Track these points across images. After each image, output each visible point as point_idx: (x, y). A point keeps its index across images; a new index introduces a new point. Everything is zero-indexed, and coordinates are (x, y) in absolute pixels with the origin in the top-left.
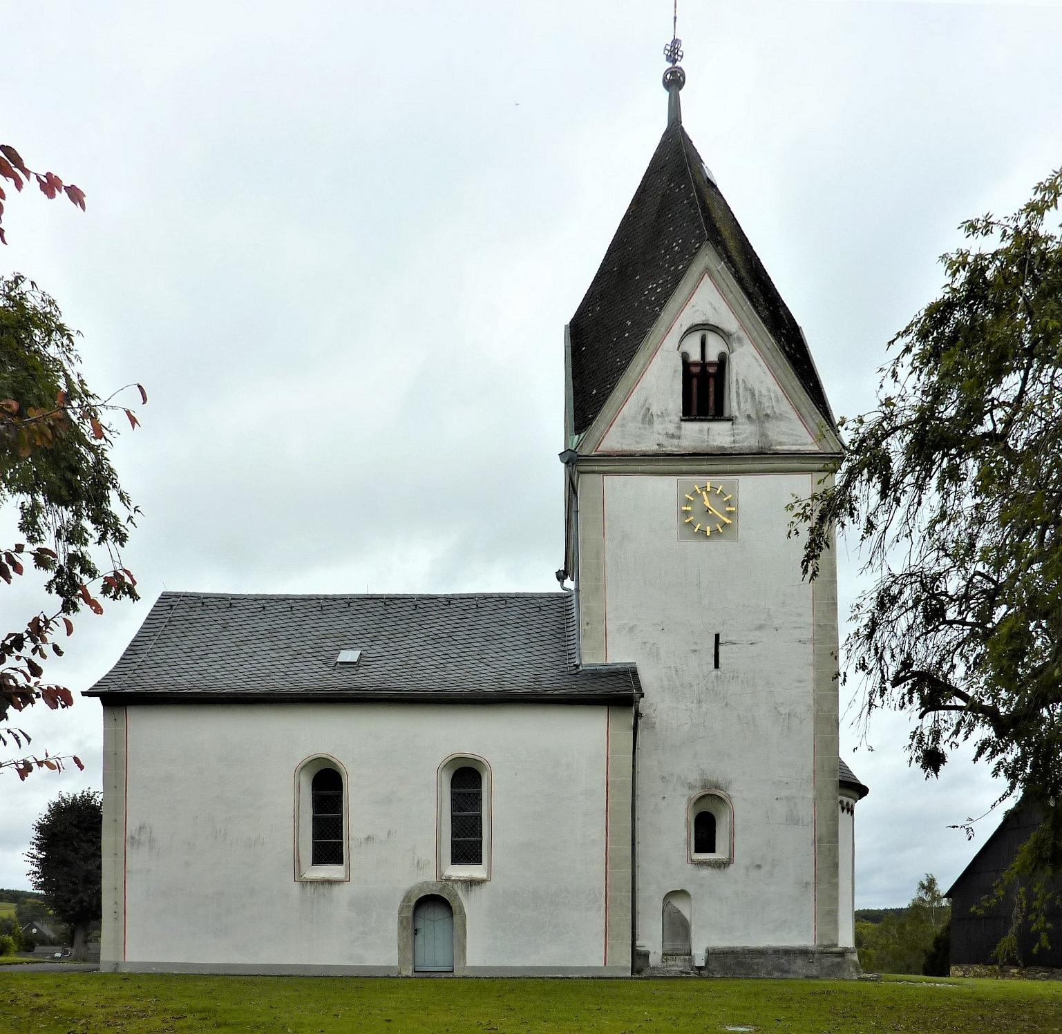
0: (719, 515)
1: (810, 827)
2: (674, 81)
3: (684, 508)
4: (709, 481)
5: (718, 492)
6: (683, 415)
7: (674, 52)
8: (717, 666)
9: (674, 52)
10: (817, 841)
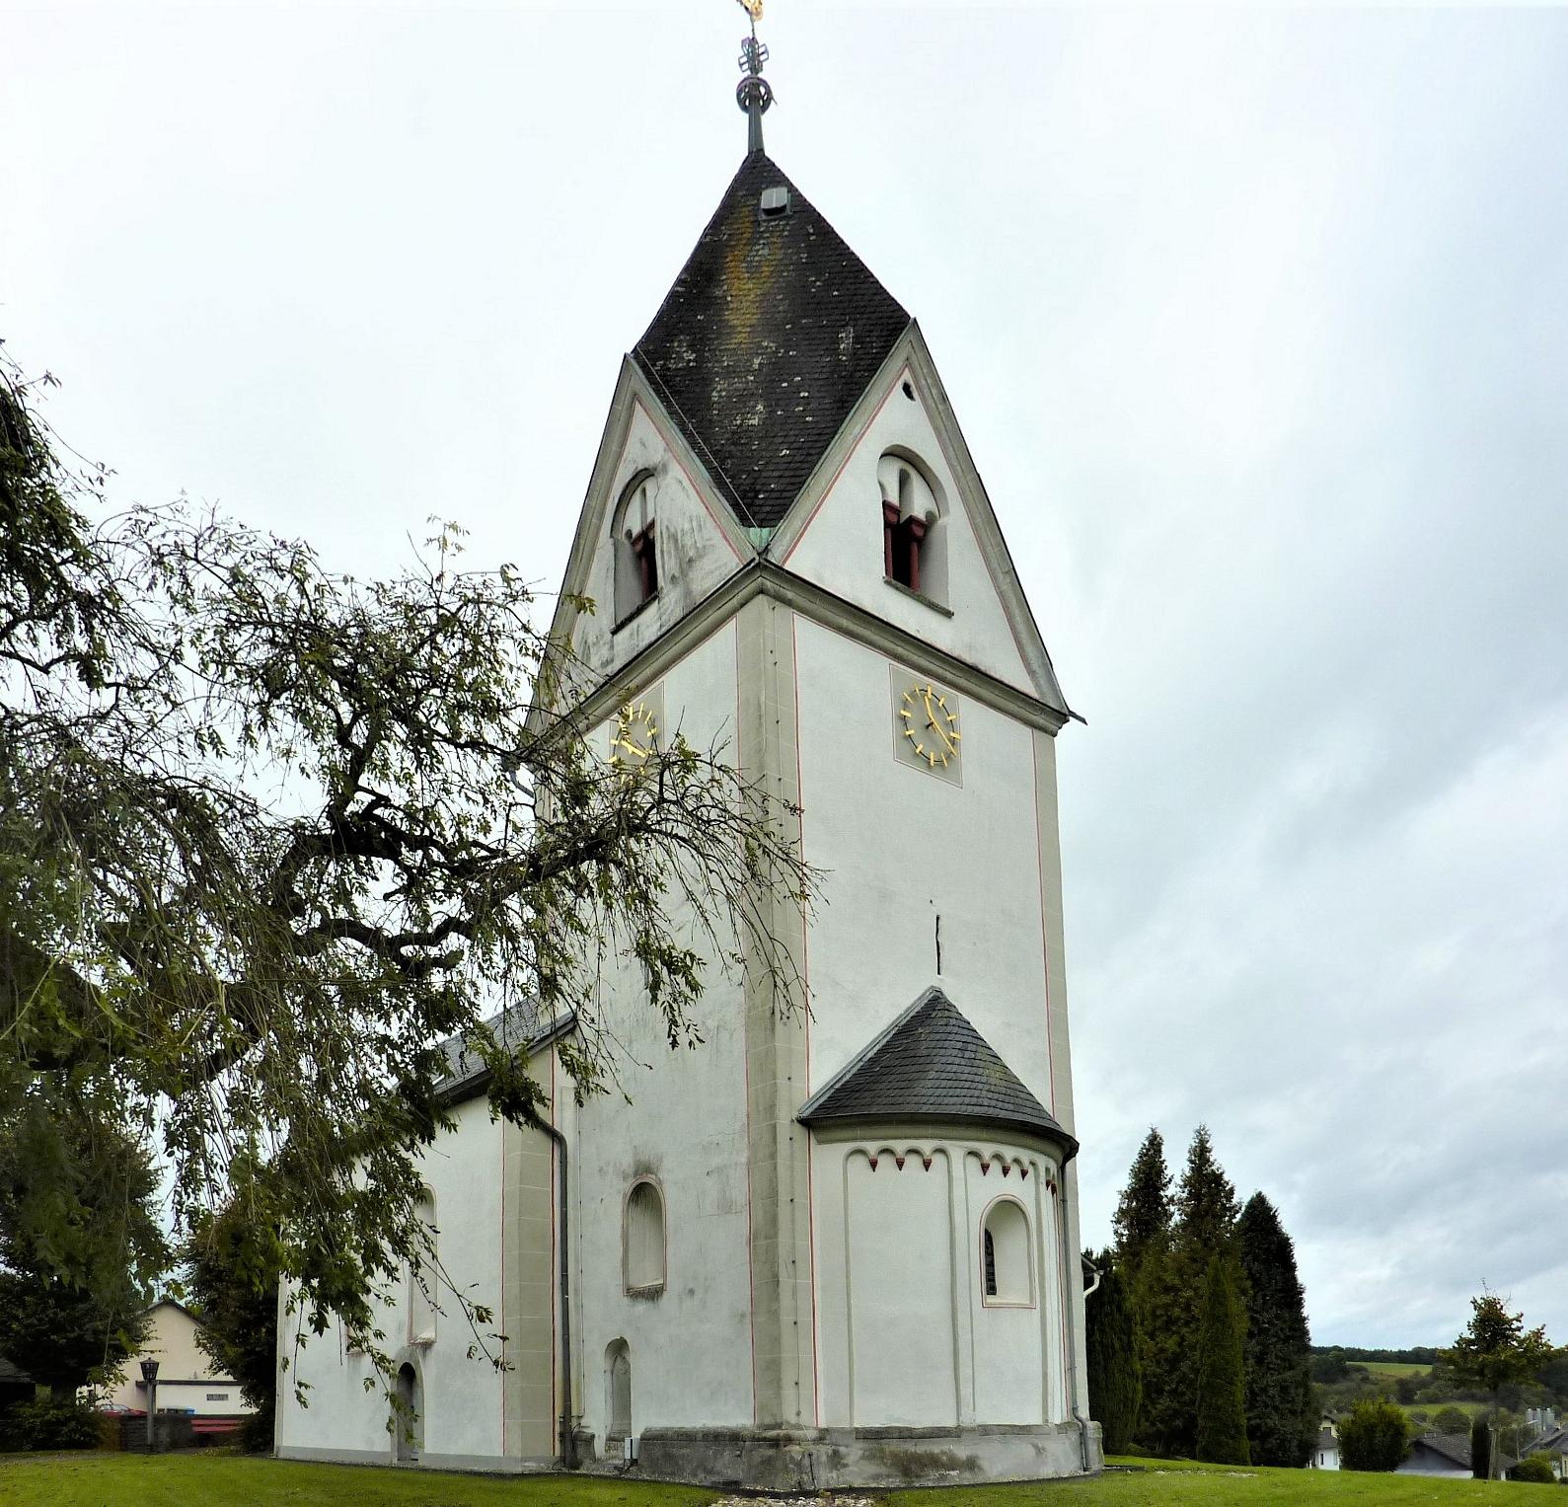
1: (744, 1214)
2: (754, 98)
4: (933, 685)
7: (754, 56)
9: (754, 56)
10: (753, 1238)
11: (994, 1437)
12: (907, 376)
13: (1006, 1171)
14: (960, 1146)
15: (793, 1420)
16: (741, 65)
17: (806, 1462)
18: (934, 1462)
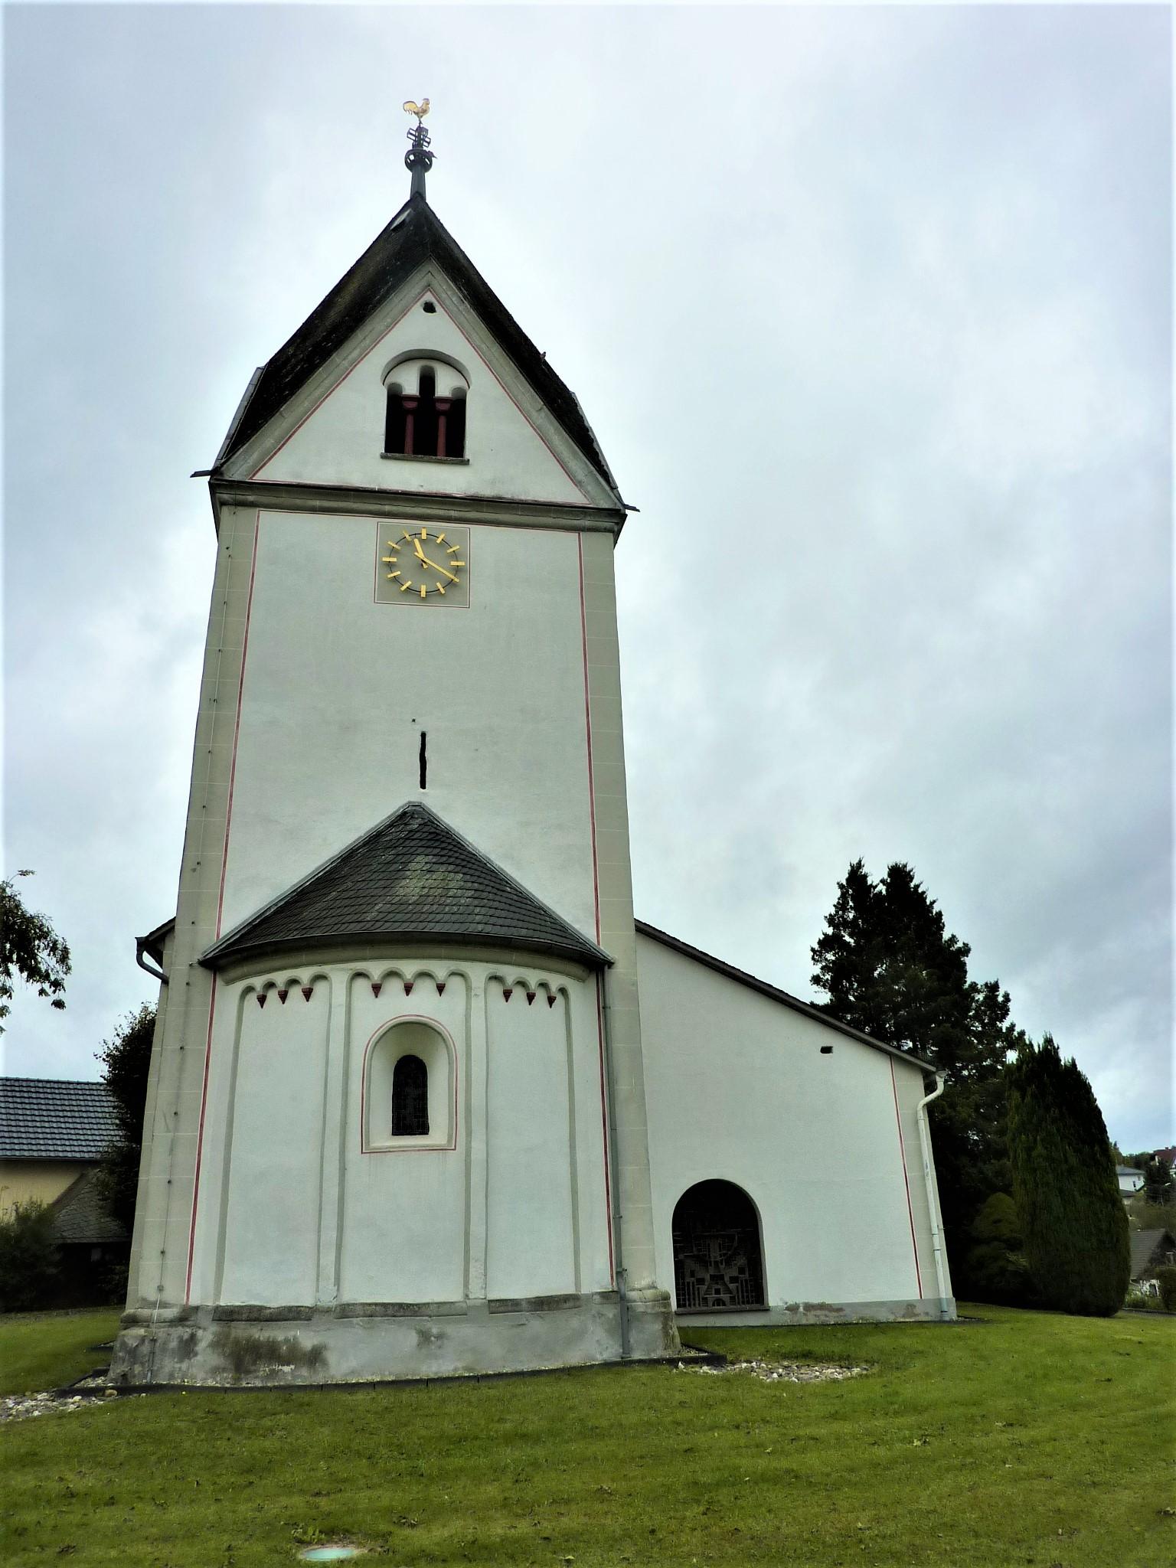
0: (445, 572)
2: (419, 161)
3: (385, 559)
4: (424, 528)
5: (438, 542)
6: (386, 451)
8: (423, 735)
11: (355, 1320)
12: (428, 297)
13: (531, 998)
14: (343, 969)
15: (152, 1295)
16: (429, 143)
17: (145, 1349)
18: (271, 1353)
